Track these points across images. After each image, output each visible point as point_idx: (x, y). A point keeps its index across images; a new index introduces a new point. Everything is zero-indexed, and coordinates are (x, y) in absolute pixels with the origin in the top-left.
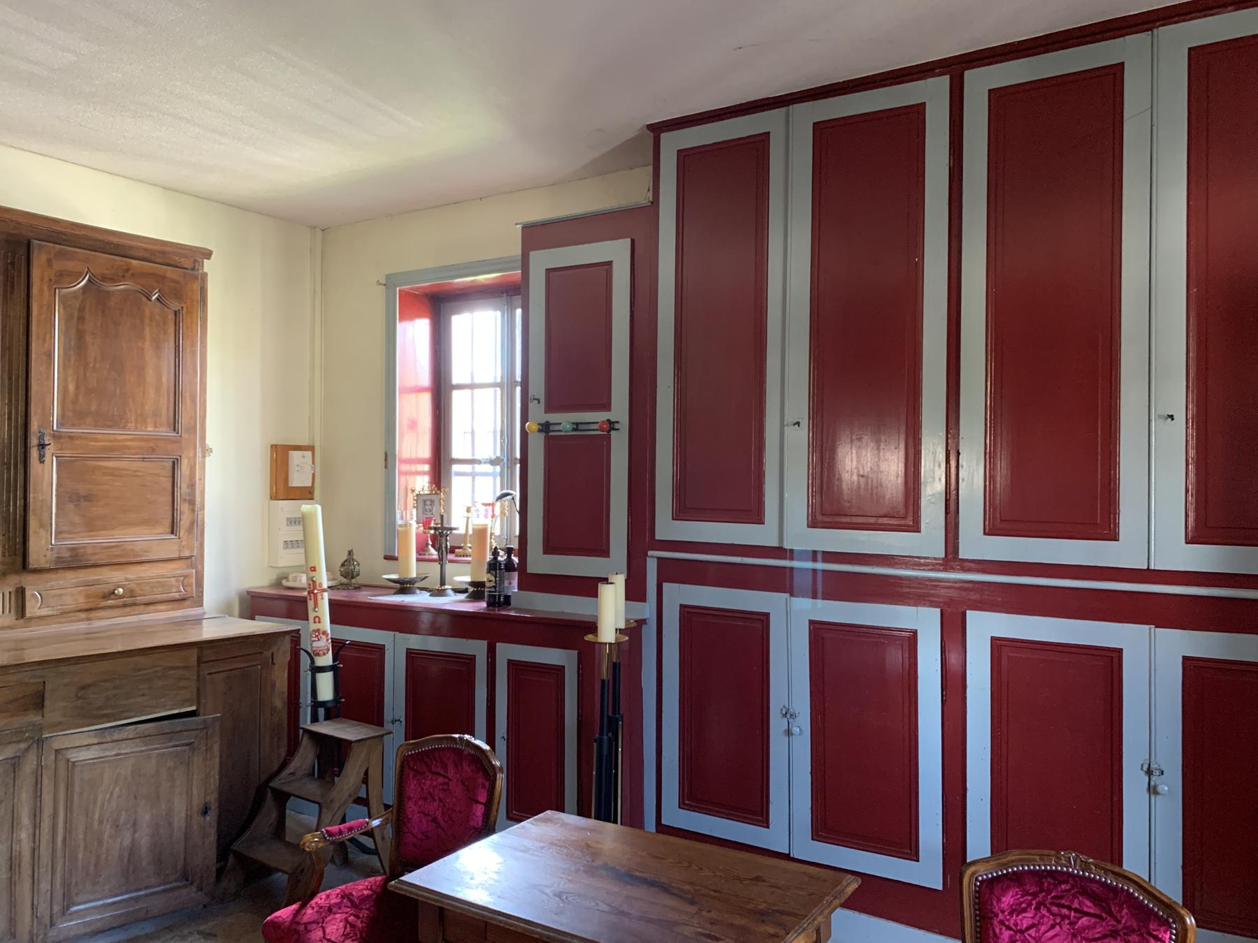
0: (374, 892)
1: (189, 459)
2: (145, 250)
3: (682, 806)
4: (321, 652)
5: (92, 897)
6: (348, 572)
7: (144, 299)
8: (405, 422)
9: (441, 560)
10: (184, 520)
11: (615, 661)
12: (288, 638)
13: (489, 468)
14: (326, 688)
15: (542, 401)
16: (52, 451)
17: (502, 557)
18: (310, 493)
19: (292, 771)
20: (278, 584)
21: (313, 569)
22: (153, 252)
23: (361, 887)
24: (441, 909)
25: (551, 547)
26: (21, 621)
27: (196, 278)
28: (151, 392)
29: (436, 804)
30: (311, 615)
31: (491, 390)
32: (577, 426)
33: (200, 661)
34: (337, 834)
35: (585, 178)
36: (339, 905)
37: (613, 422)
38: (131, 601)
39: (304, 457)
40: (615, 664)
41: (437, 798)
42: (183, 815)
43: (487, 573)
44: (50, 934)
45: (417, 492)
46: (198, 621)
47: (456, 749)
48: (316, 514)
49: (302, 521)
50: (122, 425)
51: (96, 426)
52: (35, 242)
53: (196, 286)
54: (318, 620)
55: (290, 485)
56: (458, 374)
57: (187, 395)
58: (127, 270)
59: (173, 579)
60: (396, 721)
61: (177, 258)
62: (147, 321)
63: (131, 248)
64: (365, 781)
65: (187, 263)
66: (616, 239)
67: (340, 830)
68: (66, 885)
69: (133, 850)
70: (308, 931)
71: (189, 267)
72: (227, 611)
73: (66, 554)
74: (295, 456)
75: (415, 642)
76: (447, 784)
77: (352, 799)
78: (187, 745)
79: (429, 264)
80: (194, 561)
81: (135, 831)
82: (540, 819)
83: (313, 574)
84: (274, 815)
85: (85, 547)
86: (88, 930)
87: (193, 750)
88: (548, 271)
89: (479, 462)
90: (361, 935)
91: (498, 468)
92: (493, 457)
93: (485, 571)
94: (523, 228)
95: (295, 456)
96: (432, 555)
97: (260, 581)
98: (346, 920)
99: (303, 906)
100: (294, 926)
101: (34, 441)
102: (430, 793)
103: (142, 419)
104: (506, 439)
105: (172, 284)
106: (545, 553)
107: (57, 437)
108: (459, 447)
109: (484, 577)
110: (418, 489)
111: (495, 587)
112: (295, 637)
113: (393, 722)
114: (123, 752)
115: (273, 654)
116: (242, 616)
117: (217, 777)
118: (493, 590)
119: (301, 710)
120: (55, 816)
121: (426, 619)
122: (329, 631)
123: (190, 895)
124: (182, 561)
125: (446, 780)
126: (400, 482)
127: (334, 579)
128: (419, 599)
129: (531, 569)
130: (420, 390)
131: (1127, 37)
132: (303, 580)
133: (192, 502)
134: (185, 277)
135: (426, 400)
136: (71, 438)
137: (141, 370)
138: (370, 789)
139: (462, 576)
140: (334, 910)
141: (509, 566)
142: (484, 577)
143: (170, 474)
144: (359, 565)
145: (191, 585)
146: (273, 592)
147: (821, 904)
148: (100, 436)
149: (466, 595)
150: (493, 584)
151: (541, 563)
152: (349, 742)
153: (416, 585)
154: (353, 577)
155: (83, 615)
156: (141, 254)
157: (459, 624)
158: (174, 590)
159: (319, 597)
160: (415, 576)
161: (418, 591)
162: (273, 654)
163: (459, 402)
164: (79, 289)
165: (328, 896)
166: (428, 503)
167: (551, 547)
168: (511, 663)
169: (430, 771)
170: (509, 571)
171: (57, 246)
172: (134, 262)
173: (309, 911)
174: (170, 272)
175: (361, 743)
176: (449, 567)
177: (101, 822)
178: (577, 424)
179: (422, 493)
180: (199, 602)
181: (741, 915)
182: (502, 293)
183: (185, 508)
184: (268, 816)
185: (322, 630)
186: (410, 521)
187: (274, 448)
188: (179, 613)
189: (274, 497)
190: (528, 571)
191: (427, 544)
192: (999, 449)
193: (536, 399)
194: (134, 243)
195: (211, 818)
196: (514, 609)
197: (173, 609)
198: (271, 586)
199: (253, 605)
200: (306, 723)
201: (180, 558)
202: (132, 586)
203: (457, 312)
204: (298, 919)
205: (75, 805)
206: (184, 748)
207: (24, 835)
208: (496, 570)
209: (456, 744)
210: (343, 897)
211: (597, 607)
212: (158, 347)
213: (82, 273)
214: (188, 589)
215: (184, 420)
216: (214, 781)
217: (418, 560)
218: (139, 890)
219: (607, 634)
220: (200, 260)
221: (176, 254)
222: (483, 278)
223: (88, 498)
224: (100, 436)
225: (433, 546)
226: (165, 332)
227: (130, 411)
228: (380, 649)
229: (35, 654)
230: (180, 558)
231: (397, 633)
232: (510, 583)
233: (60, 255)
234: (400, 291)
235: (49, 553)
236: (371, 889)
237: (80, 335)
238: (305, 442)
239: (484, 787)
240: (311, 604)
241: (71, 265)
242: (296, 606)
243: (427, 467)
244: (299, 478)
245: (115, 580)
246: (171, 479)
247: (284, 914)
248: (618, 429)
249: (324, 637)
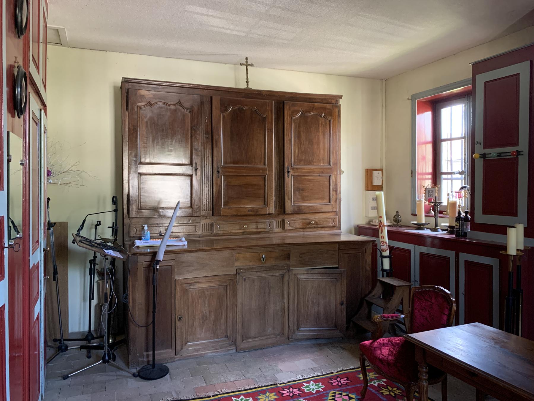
0: (401, 342)
1: (335, 175)
2: (320, 99)
4: (384, 250)
5: (306, 326)
6: (397, 220)
7: (319, 117)
8: (420, 157)
9: (435, 216)
10: (334, 198)
12: (371, 244)
13: (459, 176)
14: (386, 263)
15: (482, 144)
16: (291, 173)
17: (463, 215)
18: (381, 188)
20: (369, 223)
21: (381, 217)
22: (322, 99)
23: (396, 339)
24: (424, 349)
25: (486, 211)
26: (284, 231)
27: (336, 107)
28: (322, 151)
29: (427, 312)
30: (380, 235)
31: (460, 140)
32: (500, 155)
33: (339, 249)
35: (507, 35)
36: (387, 344)
37: (520, 152)
38: (316, 226)
39: (378, 173)
40: (518, 266)
41: (427, 310)
42: (334, 304)
43: (456, 222)
44: (294, 336)
45: (425, 187)
46: (339, 235)
48: (381, 194)
49: (376, 199)
50: (312, 163)
51: (304, 164)
52: (285, 102)
53: (337, 110)
54: (383, 237)
55: (373, 185)
56: (444, 134)
57: (334, 151)
58: (314, 107)
59: (330, 219)
61: (330, 100)
62: (320, 125)
63: (315, 99)
64: (402, 303)
65: (333, 102)
66: (522, 62)
67: (388, 316)
68: (298, 320)
69: (318, 313)
70: (375, 350)
71: (334, 103)
72: (350, 232)
73: (296, 209)
74: (375, 173)
75: (424, 249)
76: (432, 305)
77: (396, 309)
78: (336, 278)
79: (431, 87)
80: (337, 213)
81: (319, 306)
82: (471, 325)
83: (380, 219)
84: (367, 310)
85: (302, 207)
86: (305, 337)
87: (337, 281)
88: (485, 83)
89: (454, 173)
90: (395, 356)
91: (463, 176)
92: (460, 171)
93: (455, 221)
94: (473, 65)
95: (375, 173)
96: (432, 214)
97: (362, 222)
98: (390, 349)
99: (374, 341)
100: (370, 347)
101: (286, 170)
102: (424, 308)
103: (319, 161)
104: (467, 162)
105: (328, 110)
106: (483, 214)
107: (293, 169)
108: (445, 167)
109: (454, 224)
110: (426, 186)
111: (459, 228)
112: (375, 245)
113: (415, 281)
114: (314, 278)
115: (365, 249)
116: (356, 234)
117: (346, 292)
118: (458, 229)
119: (378, 273)
120: (294, 296)
121: (429, 240)
122: (387, 242)
123: (337, 333)
124: (333, 213)
125: (432, 304)
126: (418, 183)
127: (391, 223)
128: (426, 232)
129: (477, 220)
130: (426, 143)
132: (377, 223)
133: (336, 191)
134: (333, 107)
135: (430, 147)
136: (297, 169)
137: (318, 144)
138: (404, 307)
139: (445, 223)
140: (385, 345)
141: (466, 219)
142: (454, 224)
143: (329, 181)
144: (401, 217)
145: (336, 222)
146: (367, 226)
148: (306, 168)
149: (447, 232)
150: (458, 227)
151: (481, 218)
152: (395, 286)
153: (425, 226)
154: (398, 222)
155: (302, 230)
156: (318, 100)
157: (443, 243)
158: (331, 223)
159: (383, 228)
160: (424, 222)
161: (426, 229)
162: (365, 249)
163: (445, 147)
164: (298, 117)
165: (383, 340)
166: (430, 192)
167: (486, 211)
168: (466, 262)
170: (466, 222)
171: (292, 102)
172: (316, 104)
173: (376, 343)
174: (328, 106)
176: (439, 220)
177: (308, 301)
178: (500, 153)
179: (427, 187)
180: (339, 228)
182: (465, 96)
183: (334, 193)
184: (364, 310)
185: (385, 241)
186: (423, 201)
187: (367, 170)
188: (332, 232)
189: (367, 189)
190: (475, 222)
191: (430, 209)
192: (210, 177)
193: (479, 143)
194: (316, 97)
195: (344, 307)
196: (468, 238)
197: (330, 230)
198: (366, 224)
199: (359, 230)
200: (380, 277)
201: (332, 212)
202: (317, 221)
203: (443, 107)
204: (372, 345)
205: (300, 294)
206: (334, 280)
207: (285, 301)
208: (459, 221)
209: (436, 290)
210: (389, 341)
211: (506, 239)
212: (324, 134)
213: (299, 111)
214: (335, 223)
215: (333, 161)
217: (425, 216)
219: (512, 251)
220: (338, 100)
221: (330, 99)
222: (455, 90)
223: (303, 190)
224: (306, 168)
225: (433, 210)
226: (326, 128)
227: (315, 158)
228: (409, 251)
229: (288, 241)
230: (332, 212)
231: (416, 245)
232: (467, 227)
233: (293, 105)
234: (417, 101)
235: (291, 208)
236: (400, 341)
237: (299, 133)
238: (379, 167)
239: (447, 308)
240: (380, 231)
241: (296, 108)
242: (375, 232)
243: (430, 176)
244: (377, 182)
245: (311, 218)
246: (329, 183)
247: (367, 342)
248: (523, 155)
249: (385, 244)
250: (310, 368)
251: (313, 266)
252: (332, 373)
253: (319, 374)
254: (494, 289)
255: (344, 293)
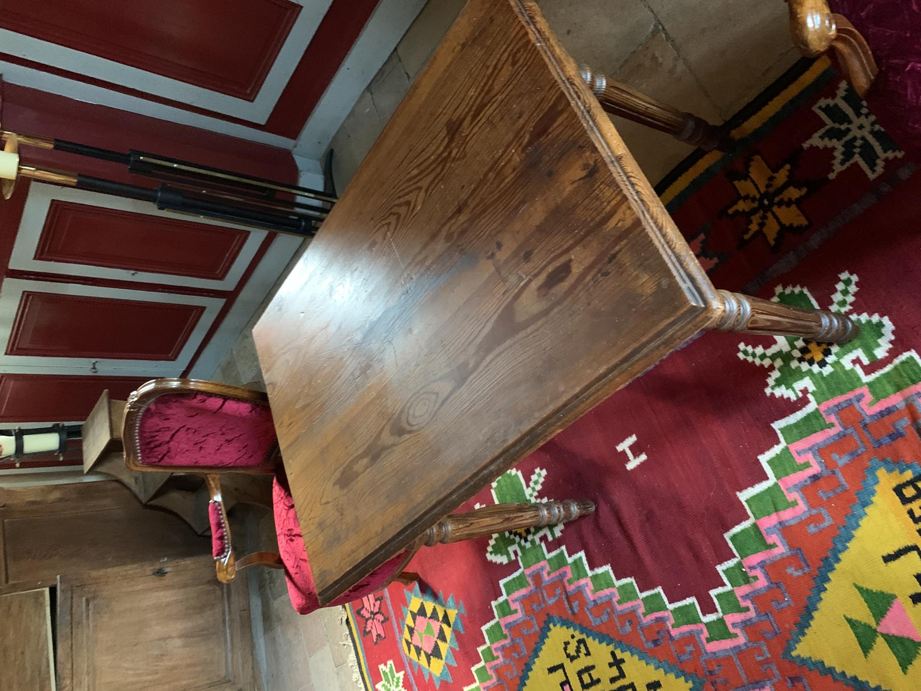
3: (252, 98)
11: (51, 146)
19: (133, 480)
34: (222, 543)
47: (145, 415)
60: (94, 368)
69: (186, 636)
78: (88, 605)
87: (94, 598)
131: (355, 103)
147: (542, 52)
169: (168, 442)
175: (114, 427)
181: (523, 202)
216: (131, 569)
218: (224, 620)
239: (204, 401)
250: (335, 669)
251: (48, 672)
252: (347, 620)
253: (352, 656)
254: (129, 210)
255: (130, 572)
